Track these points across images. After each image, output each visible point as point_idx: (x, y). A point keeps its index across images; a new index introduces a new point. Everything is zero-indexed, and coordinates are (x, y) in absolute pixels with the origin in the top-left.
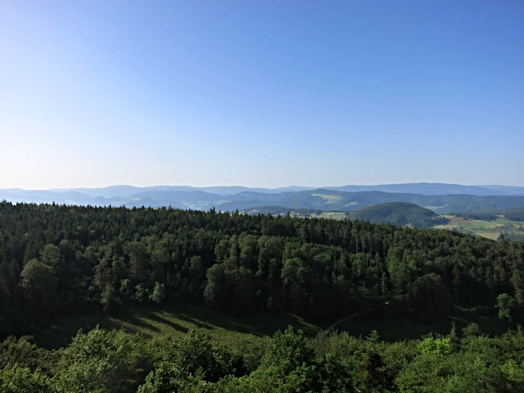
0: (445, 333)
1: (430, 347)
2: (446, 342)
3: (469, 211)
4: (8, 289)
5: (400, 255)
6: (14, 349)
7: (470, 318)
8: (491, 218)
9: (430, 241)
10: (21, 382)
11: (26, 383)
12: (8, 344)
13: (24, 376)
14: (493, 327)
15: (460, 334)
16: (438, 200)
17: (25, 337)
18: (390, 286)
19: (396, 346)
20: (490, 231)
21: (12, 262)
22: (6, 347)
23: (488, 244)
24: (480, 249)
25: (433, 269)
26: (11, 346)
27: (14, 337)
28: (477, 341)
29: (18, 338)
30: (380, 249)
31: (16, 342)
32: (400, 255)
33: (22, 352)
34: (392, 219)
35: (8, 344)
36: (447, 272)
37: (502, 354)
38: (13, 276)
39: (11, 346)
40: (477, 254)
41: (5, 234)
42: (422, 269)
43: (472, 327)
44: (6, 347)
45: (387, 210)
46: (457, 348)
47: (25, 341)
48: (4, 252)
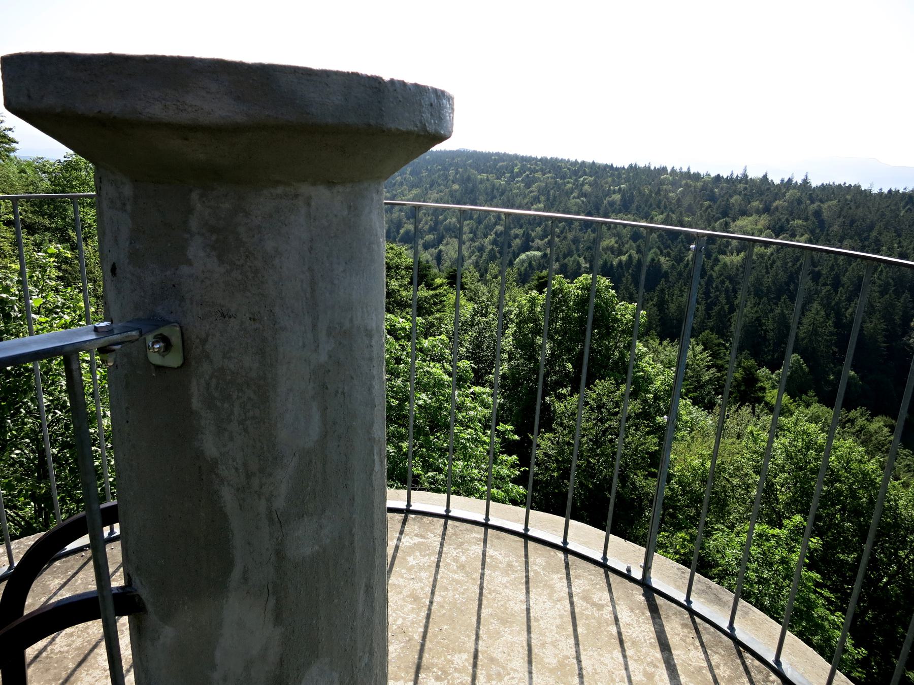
3: (53, 639)
4: (884, 342)
6: (862, 428)
10: (848, 463)
11: (854, 465)
12: (857, 418)
13: (855, 456)
17: (884, 418)
21: (902, 300)
22: (852, 421)
26: (860, 422)
27: (867, 410)
29: (873, 415)
31: (868, 420)
33: (873, 438)
35: (857, 418)
38: (898, 321)
39: (860, 422)
41: (902, 247)
44: (852, 421)
47: (882, 424)
48: (893, 279)
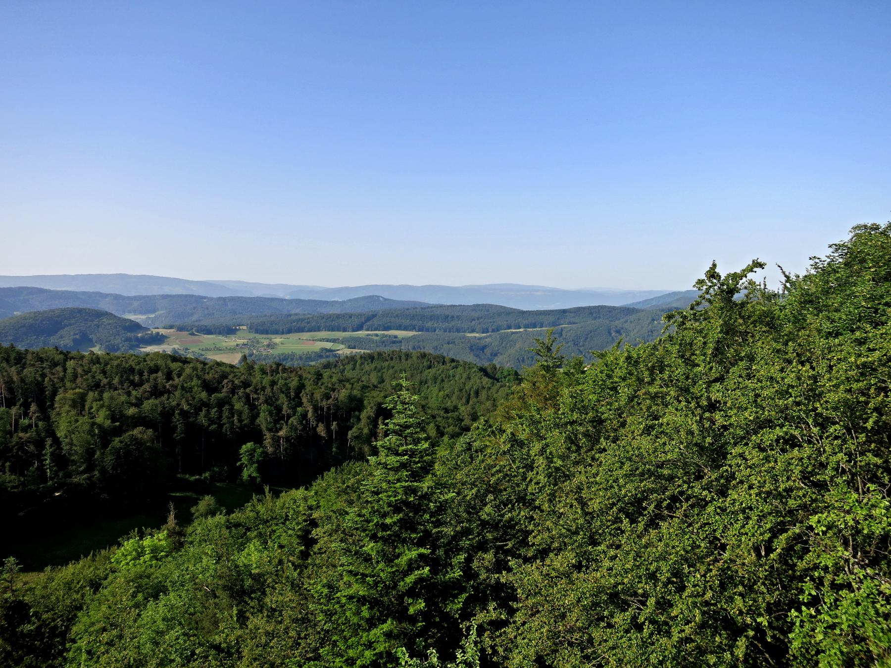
0: (158, 523)
1: (129, 555)
2: (161, 538)
5: (79, 404)
7: (202, 489)
8: (230, 331)
9: (132, 374)
14: (232, 496)
15: (185, 519)
16: (147, 303)
18: (62, 461)
19: (69, 571)
20: (227, 352)
23: (224, 372)
24: (214, 379)
25: (140, 421)
28: (208, 523)
30: (40, 396)
32: (79, 404)
34: (65, 339)
36: (162, 423)
37: (240, 534)
40: (210, 387)
42: (122, 421)
43: (207, 501)
45: (53, 322)
46: (178, 543)
